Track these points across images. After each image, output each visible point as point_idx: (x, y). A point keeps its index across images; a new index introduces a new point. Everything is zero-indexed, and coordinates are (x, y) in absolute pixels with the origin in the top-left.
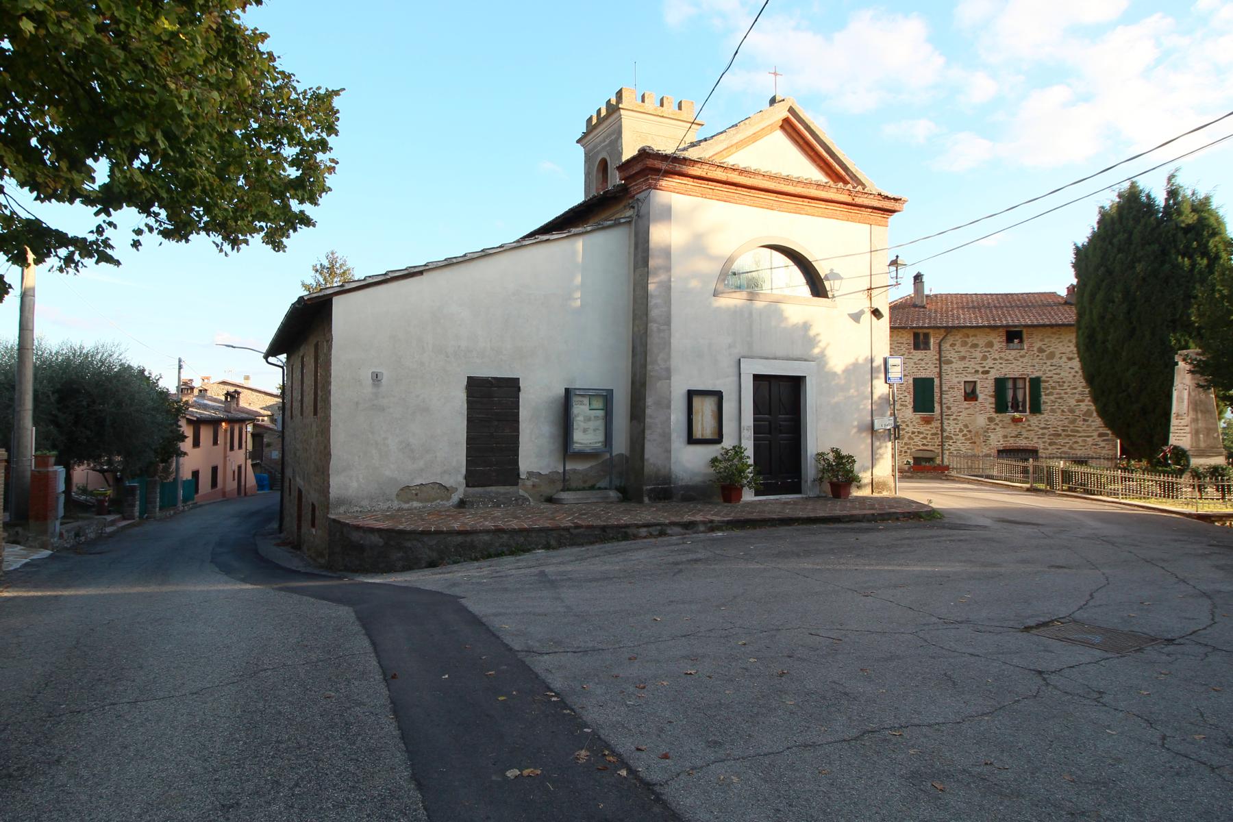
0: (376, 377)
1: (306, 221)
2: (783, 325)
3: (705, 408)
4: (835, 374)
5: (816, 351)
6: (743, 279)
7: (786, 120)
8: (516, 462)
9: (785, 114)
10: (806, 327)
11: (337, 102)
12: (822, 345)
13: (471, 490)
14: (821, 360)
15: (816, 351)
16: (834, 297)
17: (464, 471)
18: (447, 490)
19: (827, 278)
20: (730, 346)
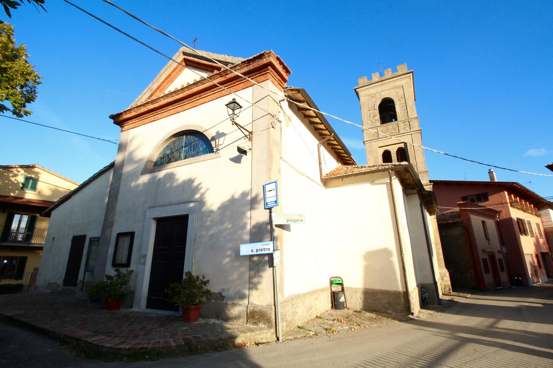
0: (54, 238)
1: (203, 194)
2: (175, 184)
3: (126, 242)
4: (212, 212)
5: (197, 196)
6: (330, 147)
7: (185, 60)
8: (11, 226)
9: (182, 57)
10: (190, 181)
11: (118, 127)
12: (202, 191)
13: (66, 287)
14: (201, 202)
15: (197, 196)
16: (218, 150)
17: (63, 278)
18: (58, 286)
19: (213, 139)
20: (144, 203)
